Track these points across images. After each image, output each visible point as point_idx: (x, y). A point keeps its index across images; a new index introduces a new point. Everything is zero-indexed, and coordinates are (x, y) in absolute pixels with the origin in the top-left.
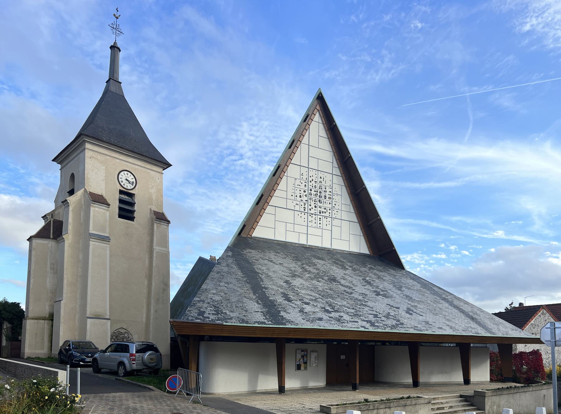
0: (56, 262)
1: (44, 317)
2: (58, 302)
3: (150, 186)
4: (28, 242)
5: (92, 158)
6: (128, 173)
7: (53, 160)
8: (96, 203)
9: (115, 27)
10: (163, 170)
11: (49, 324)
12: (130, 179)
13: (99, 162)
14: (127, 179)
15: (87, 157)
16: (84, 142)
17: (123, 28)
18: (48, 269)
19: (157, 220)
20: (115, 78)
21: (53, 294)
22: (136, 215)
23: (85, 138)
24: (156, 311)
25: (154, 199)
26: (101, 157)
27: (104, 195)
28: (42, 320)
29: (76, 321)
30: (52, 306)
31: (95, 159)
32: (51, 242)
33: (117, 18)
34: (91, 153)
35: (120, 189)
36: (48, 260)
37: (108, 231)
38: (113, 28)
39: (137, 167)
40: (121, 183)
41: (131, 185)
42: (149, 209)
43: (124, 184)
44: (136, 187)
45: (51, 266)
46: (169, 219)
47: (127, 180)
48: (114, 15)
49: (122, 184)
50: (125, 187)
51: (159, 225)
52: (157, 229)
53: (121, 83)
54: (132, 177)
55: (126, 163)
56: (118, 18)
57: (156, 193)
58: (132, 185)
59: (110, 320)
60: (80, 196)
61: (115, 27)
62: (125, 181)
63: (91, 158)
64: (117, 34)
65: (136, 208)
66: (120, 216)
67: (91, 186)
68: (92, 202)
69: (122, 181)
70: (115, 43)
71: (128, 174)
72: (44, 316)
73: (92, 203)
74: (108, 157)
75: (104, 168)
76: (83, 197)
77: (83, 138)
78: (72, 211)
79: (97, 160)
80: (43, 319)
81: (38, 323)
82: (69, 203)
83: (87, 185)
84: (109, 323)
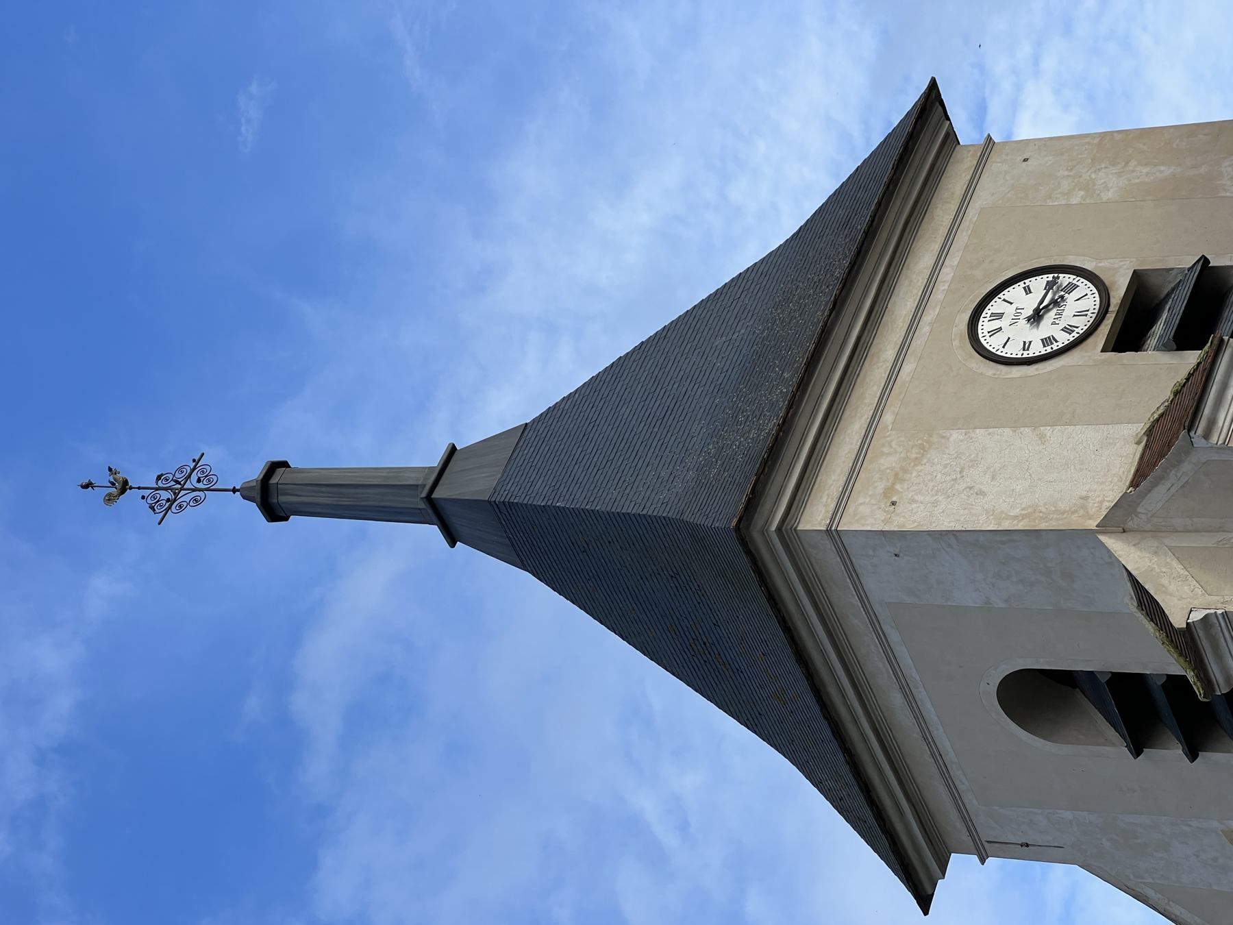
3: (1075, 200)
5: (894, 499)
6: (987, 312)
7: (924, 902)
8: (1207, 410)
9: (165, 495)
10: (959, 144)
13: (917, 462)
14: (1031, 312)
16: (787, 532)
17: (173, 460)
20: (426, 479)
23: (768, 522)
25: (1166, 171)
26: (886, 450)
27: (1140, 428)
31: (902, 481)
33: (124, 486)
34: (861, 500)
38: (175, 500)
39: (947, 274)
41: (1071, 298)
43: (1067, 330)
44: (1089, 266)
47: (1036, 317)
48: (110, 499)
53: (453, 450)
54: (1014, 293)
55: (925, 328)
56: (125, 482)
57: (1127, 163)
58: (1072, 287)
60: (1156, 553)
61: (165, 495)
62: (1047, 328)
64: (200, 486)
67: (1085, 498)
68: (1200, 431)
70: (245, 493)
73: (1207, 435)
74: (888, 418)
75: (956, 435)
76: (1167, 541)
77: (764, 532)
79: (905, 471)
82: (1206, 617)
83: (1074, 517)
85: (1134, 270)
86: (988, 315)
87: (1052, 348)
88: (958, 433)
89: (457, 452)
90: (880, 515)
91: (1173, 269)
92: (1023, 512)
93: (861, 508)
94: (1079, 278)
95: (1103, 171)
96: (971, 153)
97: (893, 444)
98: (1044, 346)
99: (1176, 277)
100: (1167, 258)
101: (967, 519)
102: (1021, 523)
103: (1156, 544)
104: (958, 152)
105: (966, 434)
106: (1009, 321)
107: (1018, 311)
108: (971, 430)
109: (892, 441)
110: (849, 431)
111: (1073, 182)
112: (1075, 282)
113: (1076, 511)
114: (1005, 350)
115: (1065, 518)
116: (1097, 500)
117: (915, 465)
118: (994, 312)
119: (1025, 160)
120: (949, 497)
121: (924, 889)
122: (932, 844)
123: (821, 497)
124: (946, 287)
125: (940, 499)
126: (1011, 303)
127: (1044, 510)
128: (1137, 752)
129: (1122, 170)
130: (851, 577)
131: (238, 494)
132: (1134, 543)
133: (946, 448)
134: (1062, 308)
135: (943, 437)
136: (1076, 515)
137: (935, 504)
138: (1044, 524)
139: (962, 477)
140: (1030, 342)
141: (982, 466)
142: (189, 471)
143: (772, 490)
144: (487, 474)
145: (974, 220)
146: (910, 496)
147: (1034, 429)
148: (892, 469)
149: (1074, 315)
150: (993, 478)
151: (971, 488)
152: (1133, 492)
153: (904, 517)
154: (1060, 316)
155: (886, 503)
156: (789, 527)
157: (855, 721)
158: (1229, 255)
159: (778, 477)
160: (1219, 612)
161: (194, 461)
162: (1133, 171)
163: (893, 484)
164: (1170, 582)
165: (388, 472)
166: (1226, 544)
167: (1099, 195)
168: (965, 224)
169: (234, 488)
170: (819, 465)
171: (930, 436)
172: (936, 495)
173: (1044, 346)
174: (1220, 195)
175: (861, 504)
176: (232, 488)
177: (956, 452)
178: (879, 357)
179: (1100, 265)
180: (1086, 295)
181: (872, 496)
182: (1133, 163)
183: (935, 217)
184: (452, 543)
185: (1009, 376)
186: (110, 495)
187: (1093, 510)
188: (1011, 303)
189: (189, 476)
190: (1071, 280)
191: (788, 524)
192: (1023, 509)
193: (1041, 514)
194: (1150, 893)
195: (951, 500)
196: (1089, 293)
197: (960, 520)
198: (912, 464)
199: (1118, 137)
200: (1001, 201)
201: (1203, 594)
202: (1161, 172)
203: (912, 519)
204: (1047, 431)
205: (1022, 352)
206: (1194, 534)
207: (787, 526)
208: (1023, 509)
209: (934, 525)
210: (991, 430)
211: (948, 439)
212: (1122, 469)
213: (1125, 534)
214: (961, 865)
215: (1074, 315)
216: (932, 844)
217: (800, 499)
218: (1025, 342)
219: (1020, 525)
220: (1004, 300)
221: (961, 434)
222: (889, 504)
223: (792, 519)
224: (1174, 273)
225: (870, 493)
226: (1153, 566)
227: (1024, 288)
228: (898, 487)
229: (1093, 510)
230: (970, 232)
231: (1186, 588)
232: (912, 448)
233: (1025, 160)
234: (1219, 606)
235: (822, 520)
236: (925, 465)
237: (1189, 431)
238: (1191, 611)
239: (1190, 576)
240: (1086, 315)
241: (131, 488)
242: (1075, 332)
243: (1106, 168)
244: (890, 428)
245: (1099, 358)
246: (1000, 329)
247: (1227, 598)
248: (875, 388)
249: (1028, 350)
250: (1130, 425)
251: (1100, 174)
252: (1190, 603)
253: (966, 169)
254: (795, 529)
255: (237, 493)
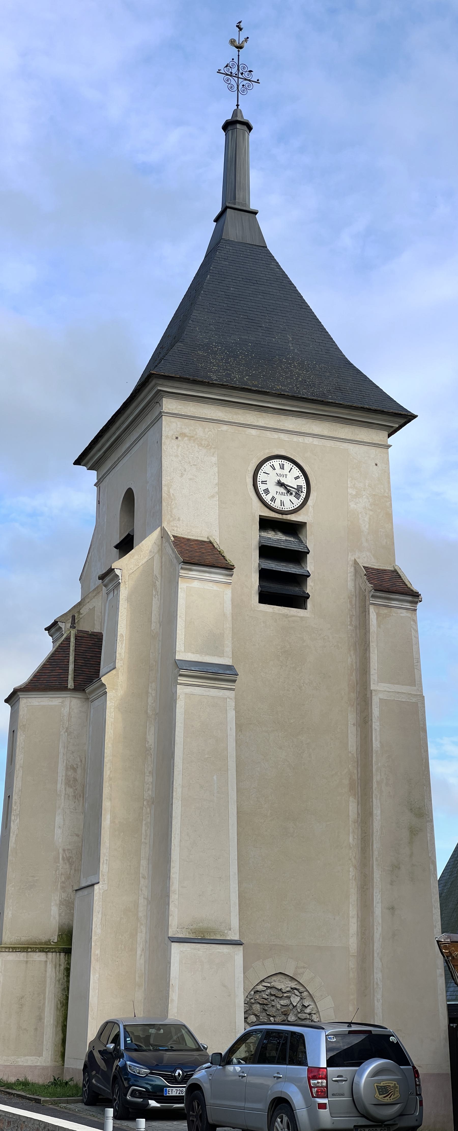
0: (81, 761)
1: (46, 943)
2: (85, 892)
3: (350, 491)
4: (8, 707)
5: (179, 438)
6: (284, 462)
7: (77, 462)
11: (60, 965)
12: (289, 481)
15: (167, 437)
18: (60, 786)
19: (378, 594)
21: (71, 864)
22: (311, 587)
23: (162, 385)
24: (392, 908)
26: (207, 430)
28: (40, 952)
29: (139, 952)
30: (68, 905)
31: (190, 440)
32: (67, 701)
34: (179, 423)
35: (260, 515)
36: (61, 756)
37: (228, 649)
39: (309, 440)
40: (264, 496)
41: (293, 498)
42: (351, 563)
43: (273, 499)
44: (310, 502)
45: (66, 775)
46: (416, 587)
47: (280, 484)
48: (232, 42)
49: (267, 498)
50: (277, 505)
51: (384, 611)
52: (379, 626)
53: (255, 213)
55: (276, 435)
56: (241, 48)
59: (241, 948)
60: (151, 552)
61: (234, 71)
62: (274, 489)
63: (177, 438)
64: (240, 87)
65: (311, 565)
66: (265, 598)
67: (179, 519)
69: (267, 491)
70: (235, 113)
71: (282, 467)
72: (44, 938)
73: (182, 568)
74: (225, 428)
75: (214, 459)
76: (157, 555)
77: (156, 385)
78: (129, 599)
80: (42, 950)
81: (27, 962)
82: (118, 576)
84: (238, 954)
85: (306, 523)
86: (283, 463)
87: (262, 494)
88: (216, 460)
89: (254, 215)
90: (170, 434)
91: (307, 539)
92: (171, 495)
93: (174, 424)
94: (303, 499)
95: (367, 500)
96: (383, 439)
97: (210, 432)
98: (264, 490)
99: (305, 540)
100: (313, 535)
101: (168, 471)
102: (166, 495)
103: (155, 551)
104: (378, 436)
105: (215, 464)
106: (279, 473)
107: (285, 476)
108: (217, 465)
109: (211, 432)
110: (217, 411)
111: (362, 488)
112: (301, 498)
113: (172, 517)
114: (262, 473)
115: (168, 513)
116: (178, 525)
117: (198, 444)
118: (285, 465)
119: (376, 465)
120: (180, 461)
121: (82, 462)
122: (97, 463)
123: (180, 405)
124: (301, 441)
125: (179, 458)
126: (289, 472)
127: (172, 503)
128: (116, 547)
129: (367, 508)
130: (152, 423)
131: (236, 107)
132: (156, 542)
133: (208, 456)
134: (286, 494)
135: (213, 454)
136: (170, 517)
137: (177, 456)
138: (165, 504)
139: (191, 466)
140: (266, 484)
141: (197, 473)
142: (249, 79)
143: (177, 384)
144: (238, 234)
145: (341, 447)
146: (181, 444)
147: (217, 493)
148: (196, 434)
149: (281, 501)
150: (190, 479)
151: (185, 470)
152: (171, 540)
153: (169, 444)
154: (281, 494)
155: (177, 434)
156: (162, 394)
157: (118, 429)
158: (313, 562)
159: (185, 385)
160: (120, 581)
161: (258, 80)
162: (366, 514)
163: (187, 436)
164: (135, 559)
165: (243, 184)
166: (155, 579)
167: (353, 501)
168: (338, 443)
169: (239, 105)
170: (198, 401)
171: (214, 448)
172: (181, 456)
173: (264, 490)
174: (349, 553)
175: (177, 424)
176: (239, 104)
177: (205, 461)
178: (260, 417)
179: (310, 507)
180: (293, 504)
181: (181, 428)
182: (371, 513)
183: (344, 429)
184: (215, 221)
185: (247, 478)
186: (235, 41)
187: (172, 524)
188: (289, 472)
189: (246, 80)
190: (302, 496)
191: (164, 394)
192: (173, 494)
193: (170, 503)
194: (90, 554)
195: (179, 463)
196: (294, 505)
197: (167, 468)
198: (198, 443)
199: (388, 504)
200: (351, 457)
201: (129, 573)
202: (365, 526)
203: (169, 448)
204: (216, 498)
205: (261, 481)
206: (160, 565)
207: (163, 393)
208: (173, 494)
209: (165, 458)
210: (217, 474)
211: (213, 456)
212: (194, 533)
213: (160, 538)
214: (93, 476)
215: (281, 501)
216: (96, 463)
217: (179, 397)
218: (266, 481)
219: (165, 494)
220: (292, 468)
221: (215, 462)
222: (177, 436)
223: (167, 395)
224: (306, 539)
225: (183, 427)
226: (144, 552)
227: (299, 476)
228: (186, 438)
229: (172, 524)
230: (333, 446)
231: (133, 566)
232: (208, 441)
233: (376, 465)
234: (123, 580)
235: (168, 408)
236: (198, 448)
237: (182, 562)
238: (121, 569)
239: (138, 567)
240: (281, 505)
241: (239, 51)
242: (271, 502)
243: (369, 501)
244: (219, 429)
245: (256, 515)
246: (274, 469)
247: (127, 583)
248: (242, 419)
249: (262, 483)
250: (218, 533)
251: (366, 499)
252: (124, 569)
253: (373, 438)
254: (163, 397)
255: (236, 107)
